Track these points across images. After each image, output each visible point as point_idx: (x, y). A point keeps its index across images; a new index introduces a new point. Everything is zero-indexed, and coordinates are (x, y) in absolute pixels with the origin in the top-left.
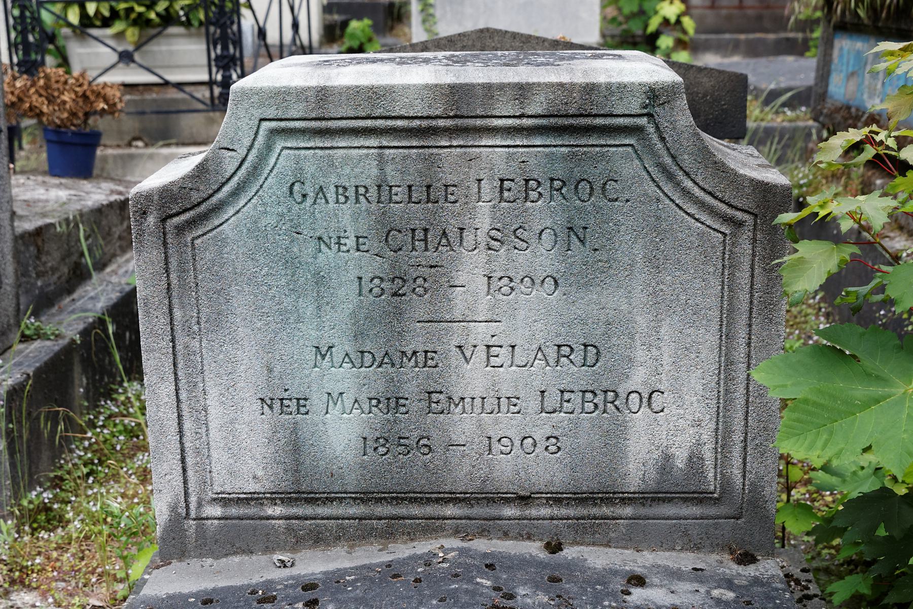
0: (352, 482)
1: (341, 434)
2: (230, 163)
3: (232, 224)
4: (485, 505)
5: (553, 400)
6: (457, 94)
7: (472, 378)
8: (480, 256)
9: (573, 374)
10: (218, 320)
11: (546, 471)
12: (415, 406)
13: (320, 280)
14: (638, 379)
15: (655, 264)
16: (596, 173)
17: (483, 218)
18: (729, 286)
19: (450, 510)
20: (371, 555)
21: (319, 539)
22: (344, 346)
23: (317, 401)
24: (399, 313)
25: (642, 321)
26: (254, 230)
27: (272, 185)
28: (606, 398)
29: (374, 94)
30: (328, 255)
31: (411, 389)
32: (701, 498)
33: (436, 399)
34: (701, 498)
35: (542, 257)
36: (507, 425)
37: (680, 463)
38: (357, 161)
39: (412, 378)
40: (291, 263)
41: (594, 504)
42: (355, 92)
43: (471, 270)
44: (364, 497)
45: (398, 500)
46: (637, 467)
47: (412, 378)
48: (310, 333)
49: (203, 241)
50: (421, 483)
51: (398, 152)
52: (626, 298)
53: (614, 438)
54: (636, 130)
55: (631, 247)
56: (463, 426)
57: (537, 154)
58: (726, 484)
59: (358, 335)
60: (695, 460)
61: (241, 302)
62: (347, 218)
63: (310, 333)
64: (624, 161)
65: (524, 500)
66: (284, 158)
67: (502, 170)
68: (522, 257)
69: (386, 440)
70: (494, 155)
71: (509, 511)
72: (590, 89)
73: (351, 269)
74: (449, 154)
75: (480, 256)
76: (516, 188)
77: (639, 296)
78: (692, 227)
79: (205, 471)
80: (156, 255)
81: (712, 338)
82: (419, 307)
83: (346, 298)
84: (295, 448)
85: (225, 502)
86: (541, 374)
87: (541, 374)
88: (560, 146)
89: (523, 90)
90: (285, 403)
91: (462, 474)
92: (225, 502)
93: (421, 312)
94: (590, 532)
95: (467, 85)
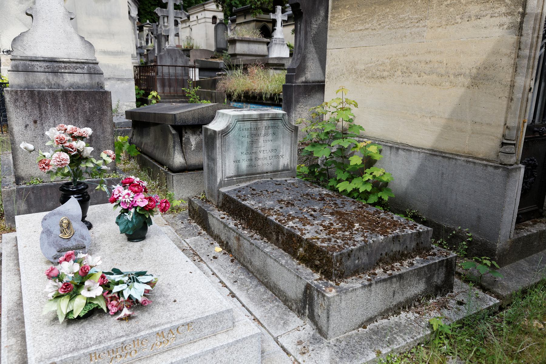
0: (245, 173)
1: (244, 165)
2: (231, 126)
3: (231, 135)
4: (262, 174)
5: (271, 158)
6: (261, 115)
7: (261, 155)
8: (263, 138)
9: (273, 154)
10: (228, 150)
11: (270, 168)
12: (254, 160)
13: (242, 142)
14: (281, 154)
15: (283, 137)
16: (277, 125)
17: (263, 133)
18: (292, 140)
19: (258, 175)
20: (248, 183)
21: (240, 182)
22: (245, 152)
23: (241, 160)
24: (252, 146)
25: (282, 146)
26: (234, 136)
27: (237, 129)
28: (277, 157)
29: (250, 115)
30: (243, 139)
31: (253, 158)
32: (288, 170)
33: (257, 159)
34: (288, 170)
35: (270, 137)
36: (265, 162)
37: (286, 164)
38: (248, 125)
39: (254, 156)
40: (238, 140)
41: (276, 172)
42: (248, 115)
43: (261, 139)
44: (247, 175)
45: (251, 175)
46: (281, 167)
47: (254, 156)
48: (241, 150)
49: (227, 137)
50: (254, 172)
51: (253, 123)
52: (280, 142)
53: (278, 162)
54: (281, 119)
55: (280, 135)
56: (260, 163)
57: (269, 123)
58: (291, 167)
59: (247, 150)
60: (288, 164)
61: (232, 146)
62: (246, 133)
63: (241, 150)
64: (280, 123)
65: (267, 173)
66: (238, 125)
67: (266, 125)
68: (268, 137)
69: (250, 166)
70: (265, 123)
71: (265, 175)
72: (276, 114)
73: (246, 140)
74: (259, 123)
75: (263, 138)
76: (267, 128)
77: (281, 142)
78: (287, 132)
79: (225, 173)
80: (220, 140)
81: (290, 147)
82: (255, 146)
83: (246, 145)
84: (238, 168)
85: (227, 178)
86: (270, 154)
87: (270, 154)
88: (272, 122)
89: (268, 114)
90: (237, 161)
91: (259, 170)
92: (227, 178)
93: (255, 146)
94: (275, 176)
95: (148, 113)
